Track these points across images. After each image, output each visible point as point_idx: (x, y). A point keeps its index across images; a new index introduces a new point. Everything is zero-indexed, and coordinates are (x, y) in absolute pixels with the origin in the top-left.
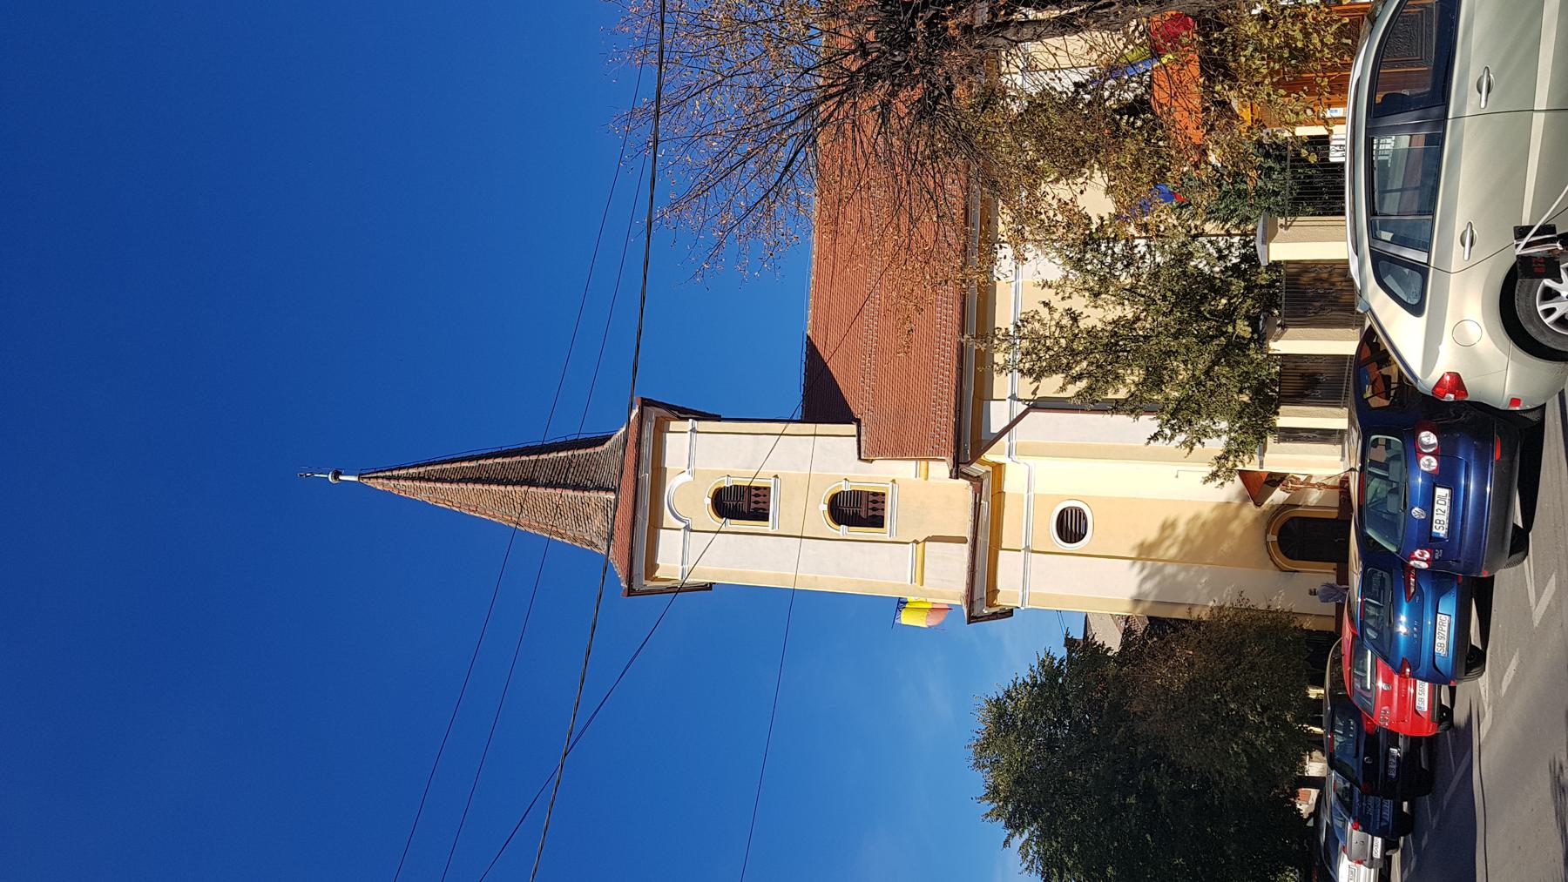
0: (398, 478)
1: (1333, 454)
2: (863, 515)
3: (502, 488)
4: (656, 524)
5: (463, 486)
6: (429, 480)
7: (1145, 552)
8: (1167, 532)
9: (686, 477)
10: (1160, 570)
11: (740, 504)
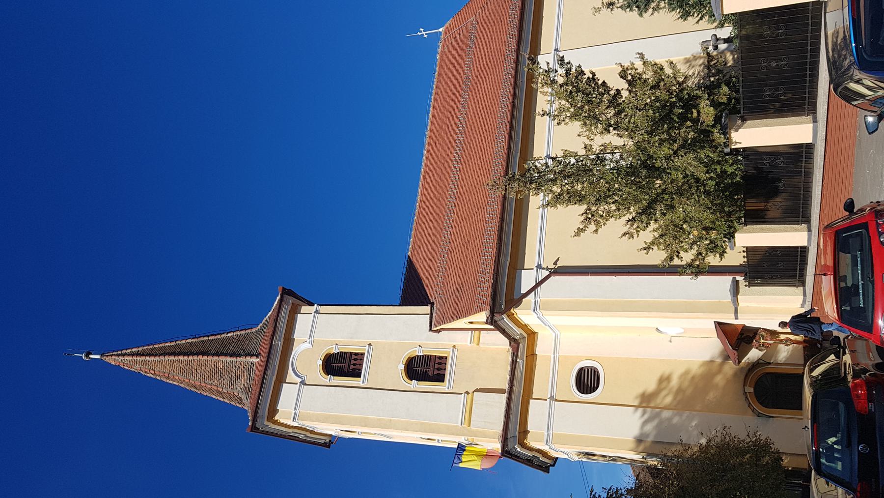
0: (124, 355)
1: (797, 295)
2: (430, 373)
3: (186, 358)
4: (281, 379)
5: (162, 358)
6: (143, 355)
7: (646, 400)
8: (664, 384)
9: (307, 345)
10: (657, 415)
11: (342, 365)
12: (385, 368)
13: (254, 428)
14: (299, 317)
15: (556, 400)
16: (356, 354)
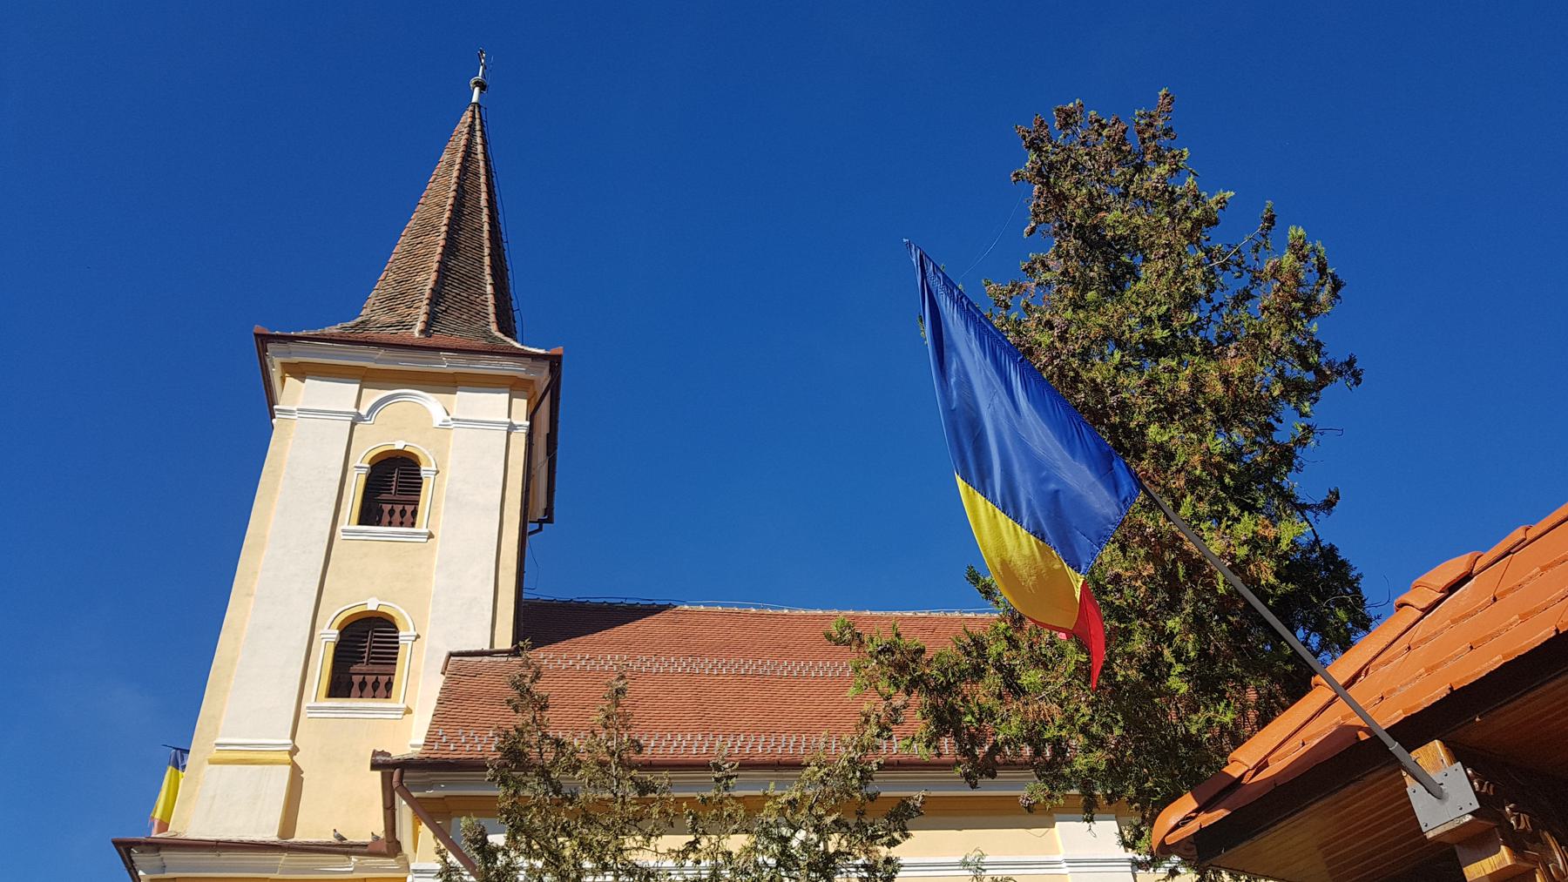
4: (367, 378)
11: (391, 488)
12: (375, 572)
13: (263, 340)
14: (504, 397)
16: (414, 513)
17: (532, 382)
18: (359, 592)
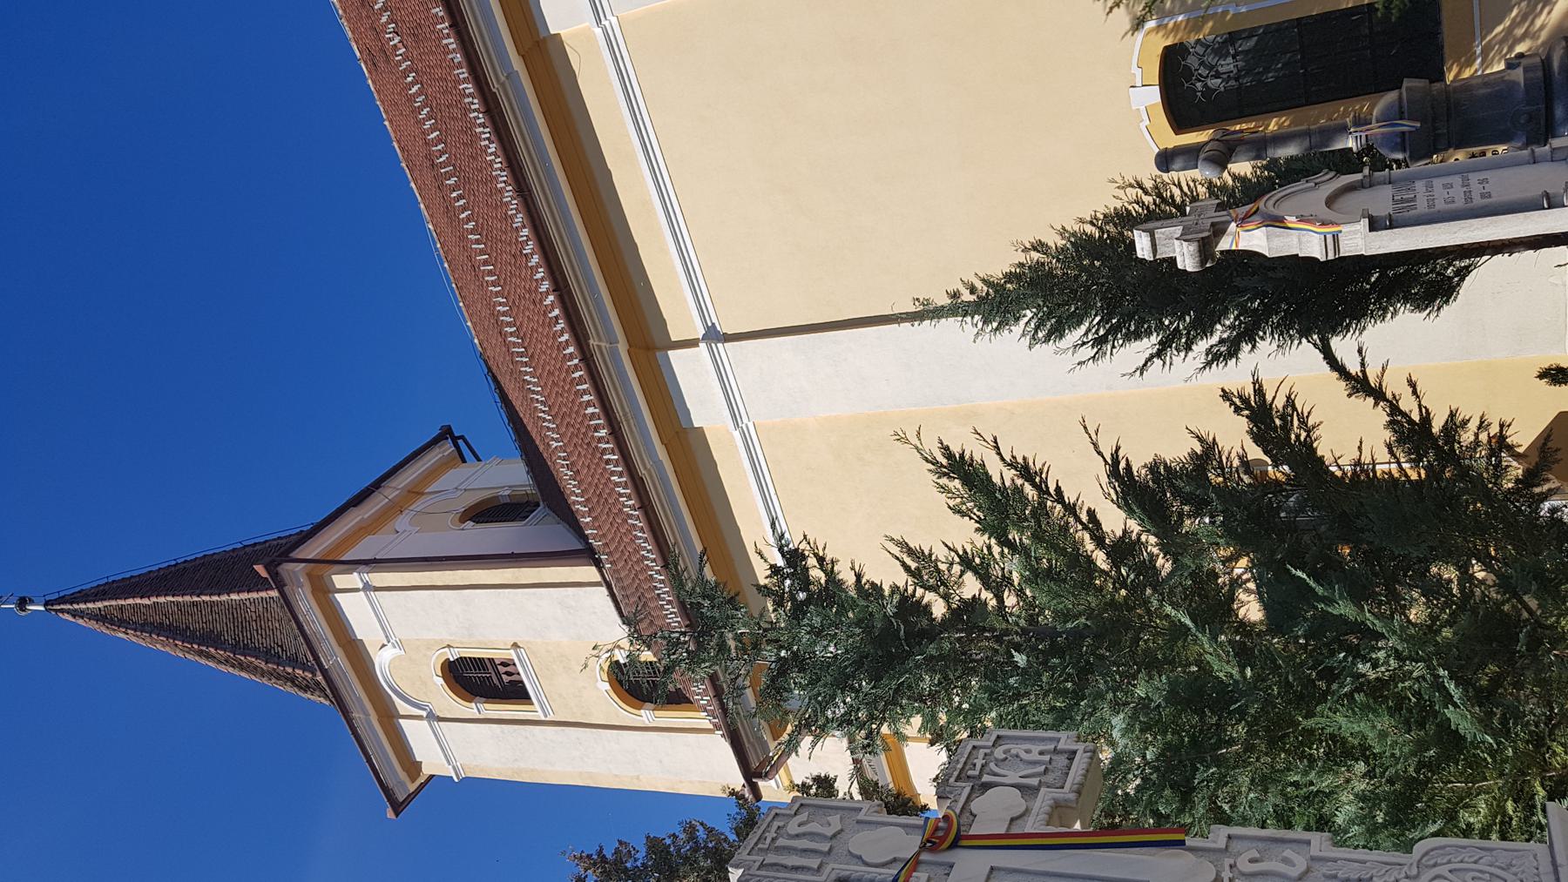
4: (389, 717)
15: (728, 338)
17: (310, 576)
18: (602, 700)
